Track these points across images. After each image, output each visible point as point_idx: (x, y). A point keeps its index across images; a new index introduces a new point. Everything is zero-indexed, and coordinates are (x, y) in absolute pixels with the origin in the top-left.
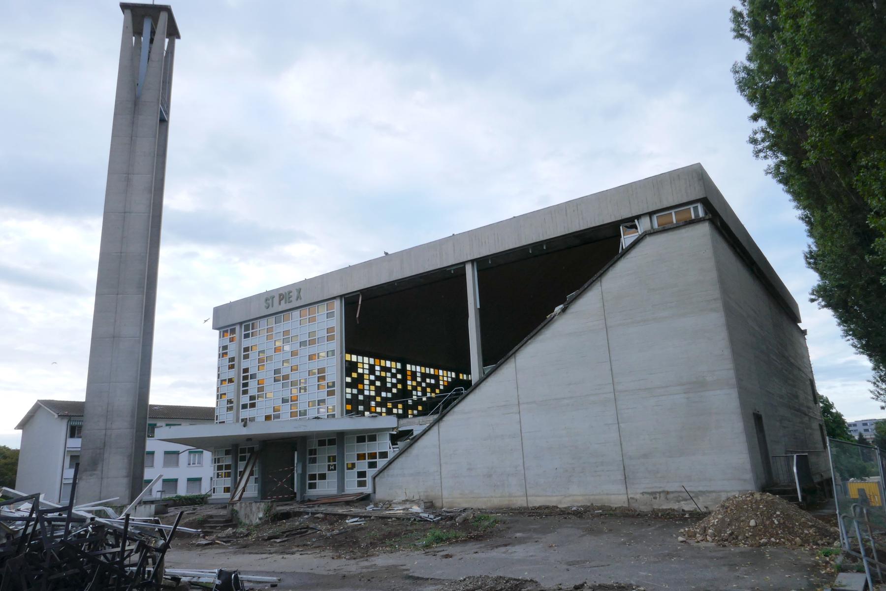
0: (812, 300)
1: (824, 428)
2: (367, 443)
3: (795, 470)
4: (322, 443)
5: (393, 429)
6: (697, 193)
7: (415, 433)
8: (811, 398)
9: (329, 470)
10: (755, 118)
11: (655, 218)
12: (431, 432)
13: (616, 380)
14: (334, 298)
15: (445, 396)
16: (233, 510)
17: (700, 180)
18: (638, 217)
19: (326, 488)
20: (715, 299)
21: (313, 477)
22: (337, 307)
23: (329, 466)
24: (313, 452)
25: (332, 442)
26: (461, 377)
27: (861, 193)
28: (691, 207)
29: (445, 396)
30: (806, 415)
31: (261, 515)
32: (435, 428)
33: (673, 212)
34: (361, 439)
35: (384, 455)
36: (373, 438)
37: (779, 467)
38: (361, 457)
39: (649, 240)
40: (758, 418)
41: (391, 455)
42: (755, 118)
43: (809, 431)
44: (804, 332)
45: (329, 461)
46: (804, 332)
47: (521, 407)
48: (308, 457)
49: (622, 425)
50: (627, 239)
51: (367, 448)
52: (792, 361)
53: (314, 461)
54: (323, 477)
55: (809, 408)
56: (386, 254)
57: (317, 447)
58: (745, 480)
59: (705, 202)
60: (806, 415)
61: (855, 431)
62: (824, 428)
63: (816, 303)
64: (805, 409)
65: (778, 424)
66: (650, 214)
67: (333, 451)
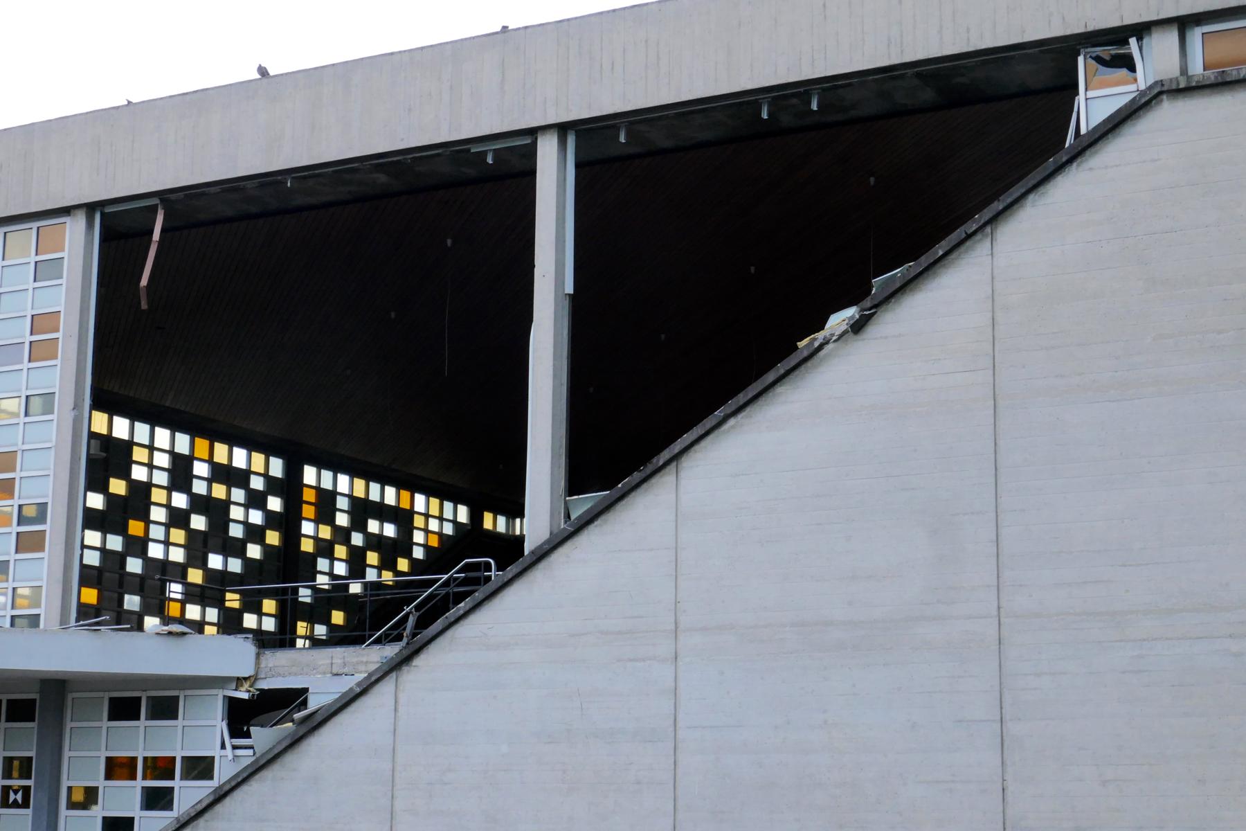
2: (143, 722)
11: (1196, 36)
14: (66, 211)
15: (430, 583)
18: (1141, 30)
22: (77, 245)
29: (430, 583)
35: (200, 767)
36: (166, 709)
38: (118, 768)
41: (224, 771)
50: (1096, 101)
51: (144, 739)
56: (263, 72)
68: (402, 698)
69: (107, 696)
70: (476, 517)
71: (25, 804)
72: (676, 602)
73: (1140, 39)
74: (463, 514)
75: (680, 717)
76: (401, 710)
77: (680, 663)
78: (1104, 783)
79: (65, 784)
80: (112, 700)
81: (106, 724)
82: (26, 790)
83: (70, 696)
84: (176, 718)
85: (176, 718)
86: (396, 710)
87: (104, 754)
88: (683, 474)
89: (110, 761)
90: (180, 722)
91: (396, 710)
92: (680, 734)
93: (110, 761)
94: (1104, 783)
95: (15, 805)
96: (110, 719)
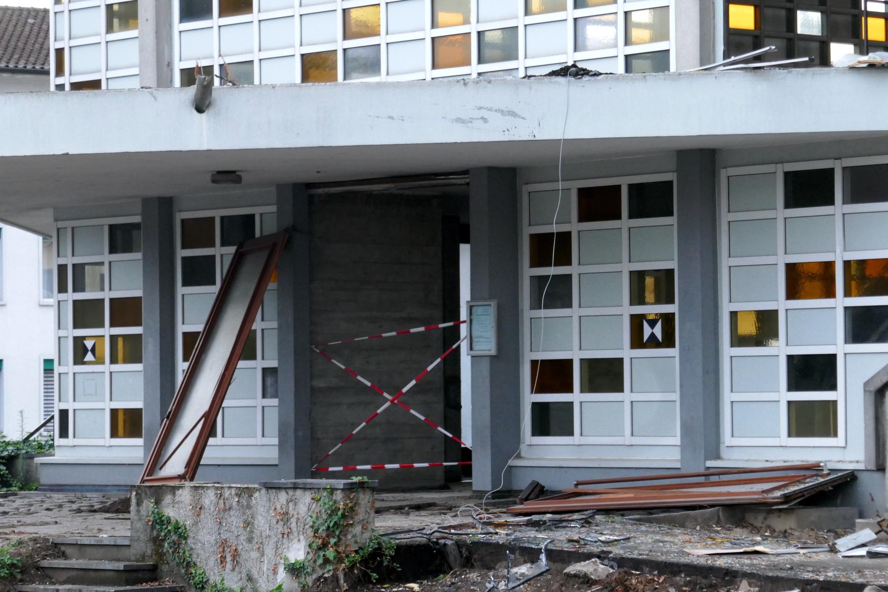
2: (839, 208)
4: (598, 204)
9: (637, 342)
16: (160, 521)
19: (627, 431)
21: (554, 375)
23: (637, 322)
24: (553, 248)
25: (651, 200)
31: (297, 552)
38: (805, 281)
40: (873, 500)
48: (528, 272)
54: (606, 375)
57: (574, 227)
67: (657, 244)
69: (780, 170)
71: (668, 341)
80: (787, 174)
81: (782, 212)
82: (668, 320)
83: (724, 174)
95: (653, 343)
96: (788, 205)
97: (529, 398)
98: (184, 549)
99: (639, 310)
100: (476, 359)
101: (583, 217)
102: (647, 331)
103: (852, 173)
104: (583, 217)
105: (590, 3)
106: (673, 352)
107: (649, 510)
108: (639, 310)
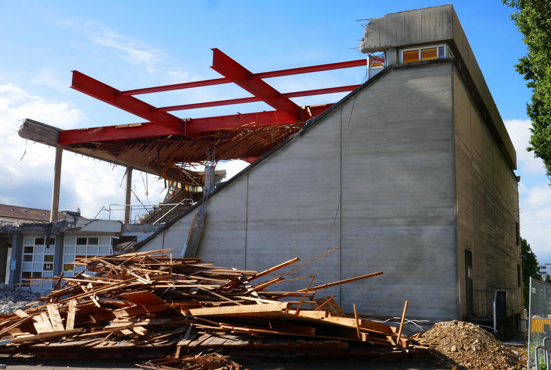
0: (530, 150)
1: (521, 268)
2: (87, 245)
3: (494, 305)
5: (116, 234)
6: (443, 33)
7: (139, 240)
8: (514, 240)
9: (45, 269)
10: (36, 322)
11: (402, 52)
12: (155, 240)
13: (343, 207)
15: (172, 206)
17: (449, 21)
20: (446, 140)
21: (27, 275)
23: (45, 265)
26: (187, 189)
27: (52, 231)
28: (438, 46)
29: (172, 206)
30: (508, 255)
32: (160, 237)
33: (419, 49)
34: (82, 241)
36: (94, 241)
37: (480, 300)
39: (393, 75)
40: (468, 254)
42: (36, 322)
43: (508, 270)
44: (518, 179)
45: (45, 260)
46: (518, 179)
47: (249, 224)
49: (344, 251)
52: (504, 203)
53: (29, 258)
54: (38, 275)
55: (511, 248)
58: (449, 310)
59: (451, 43)
60: (508, 255)
61: (544, 273)
62: (521, 268)
63: (533, 152)
64: (507, 249)
65: (484, 261)
66: (398, 49)
68: (165, 240)
70: (183, 186)
71: (51, 269)
72: (247, 213)
73: (398, 62)
74: (179, 186)
75: (247, 246)
76: (165, 243)
77: (248, 230)
78: (369, 267)
79: (64, 263)
80: (78, 239)
82: (52, 265)
83: (65, 238)
84: (97, 244)
85: (97, 244)
86: (163, 243)
87: (44, 254)
88: (250, 176)
89: (46, 256)
90: (98, 246)
91: (163, 243)
92: (248, 251)
93: (46, 256)
94: (369, 267)
95: (48, 269)
97: (24, 254)
98: (444, 324)
99: (46, 263)
100: (11, 271)
101: (36, 244)
102: (47, 267)
103: (90, 239)
104: (36, 244)
105: (57, 132)
106: (52, 271)
107: (455, 181)
108: (46, 263)
